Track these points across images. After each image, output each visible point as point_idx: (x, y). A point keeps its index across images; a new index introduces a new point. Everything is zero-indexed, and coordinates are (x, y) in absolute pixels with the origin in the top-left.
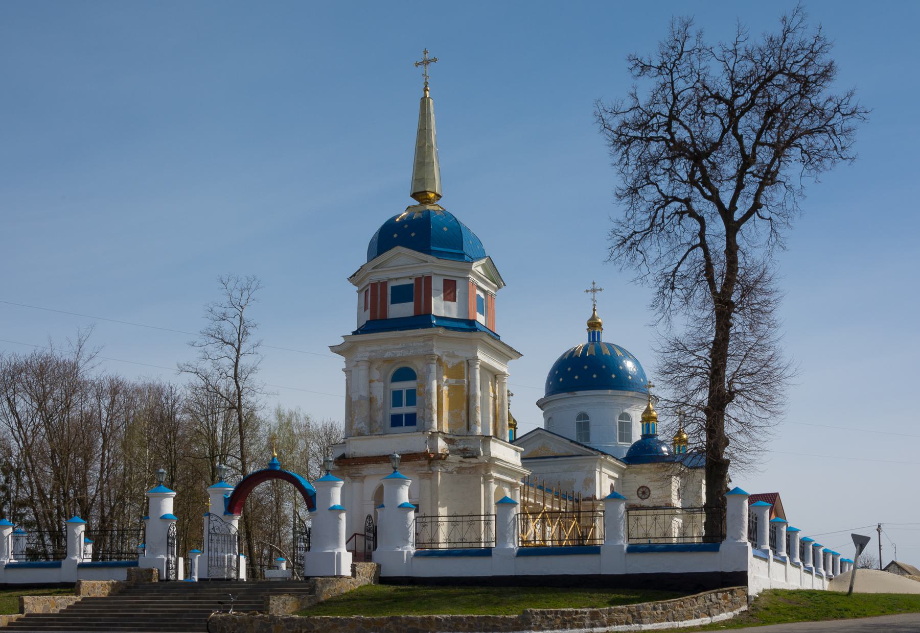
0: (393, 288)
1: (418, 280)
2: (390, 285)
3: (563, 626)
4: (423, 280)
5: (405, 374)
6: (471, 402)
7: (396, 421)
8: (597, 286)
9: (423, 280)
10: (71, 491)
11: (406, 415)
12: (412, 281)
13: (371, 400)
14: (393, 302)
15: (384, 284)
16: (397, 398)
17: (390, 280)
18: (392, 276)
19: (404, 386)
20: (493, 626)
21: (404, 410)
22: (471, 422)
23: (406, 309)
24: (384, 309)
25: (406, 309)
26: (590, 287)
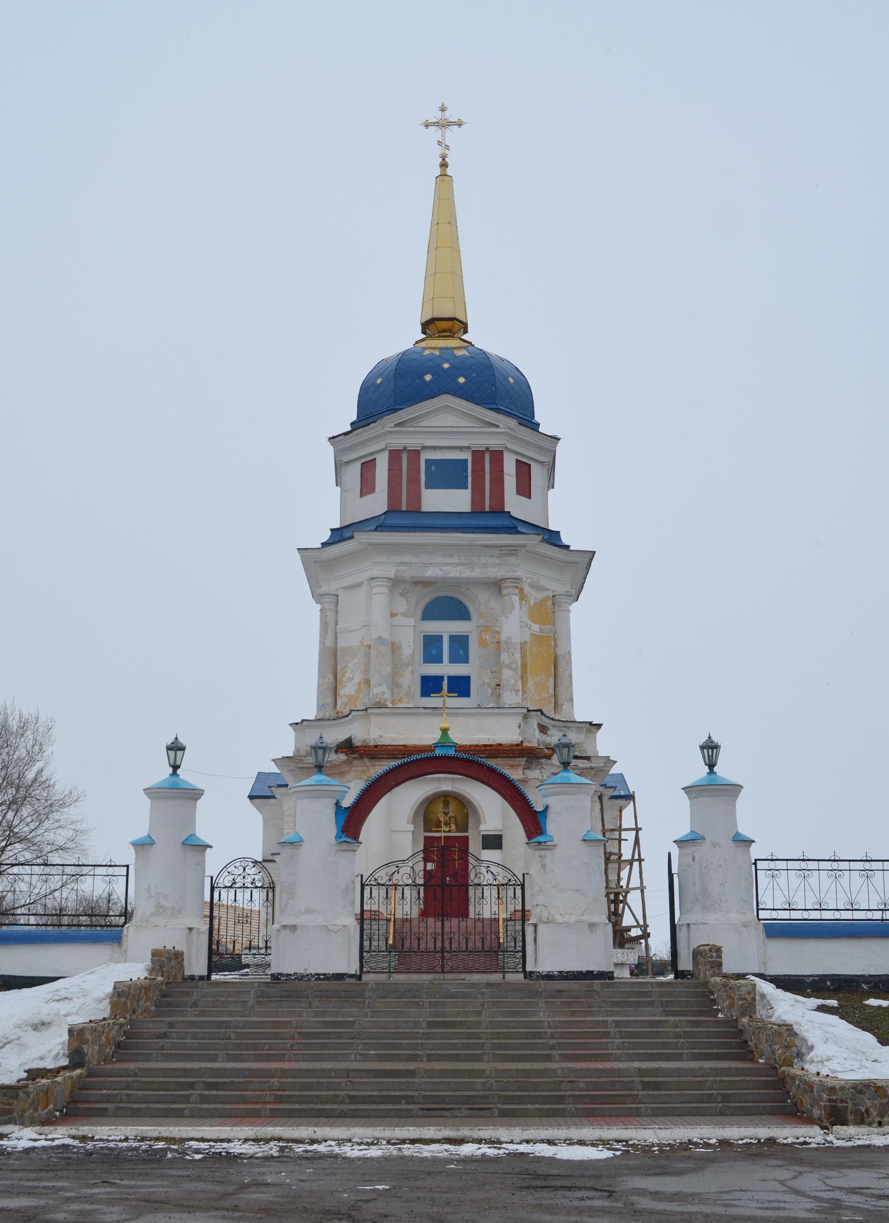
0: (427, 460)
1: (478, 455)
2: (425, 456)
3: (824, 978)
4: (487, 457)
5: (447, 605)
6: (562, 665)
7: (430, 685)
8: (452, 115)
9: (487, 457)
10: (38, 792)
11: (450, 678)
12: (467, 456)
13: (395, 648)
14: (427, 488)
15: (414, 455)
16: (431, 648)
17: (425, 448)
18: (428, 443)
19: (446, 628)
20: (28, 1154)
21: (446, 669)
22: (562, 697)
23: (458, 500)
24: (415, 496)
25: (458, 500)
26: (435, 115)
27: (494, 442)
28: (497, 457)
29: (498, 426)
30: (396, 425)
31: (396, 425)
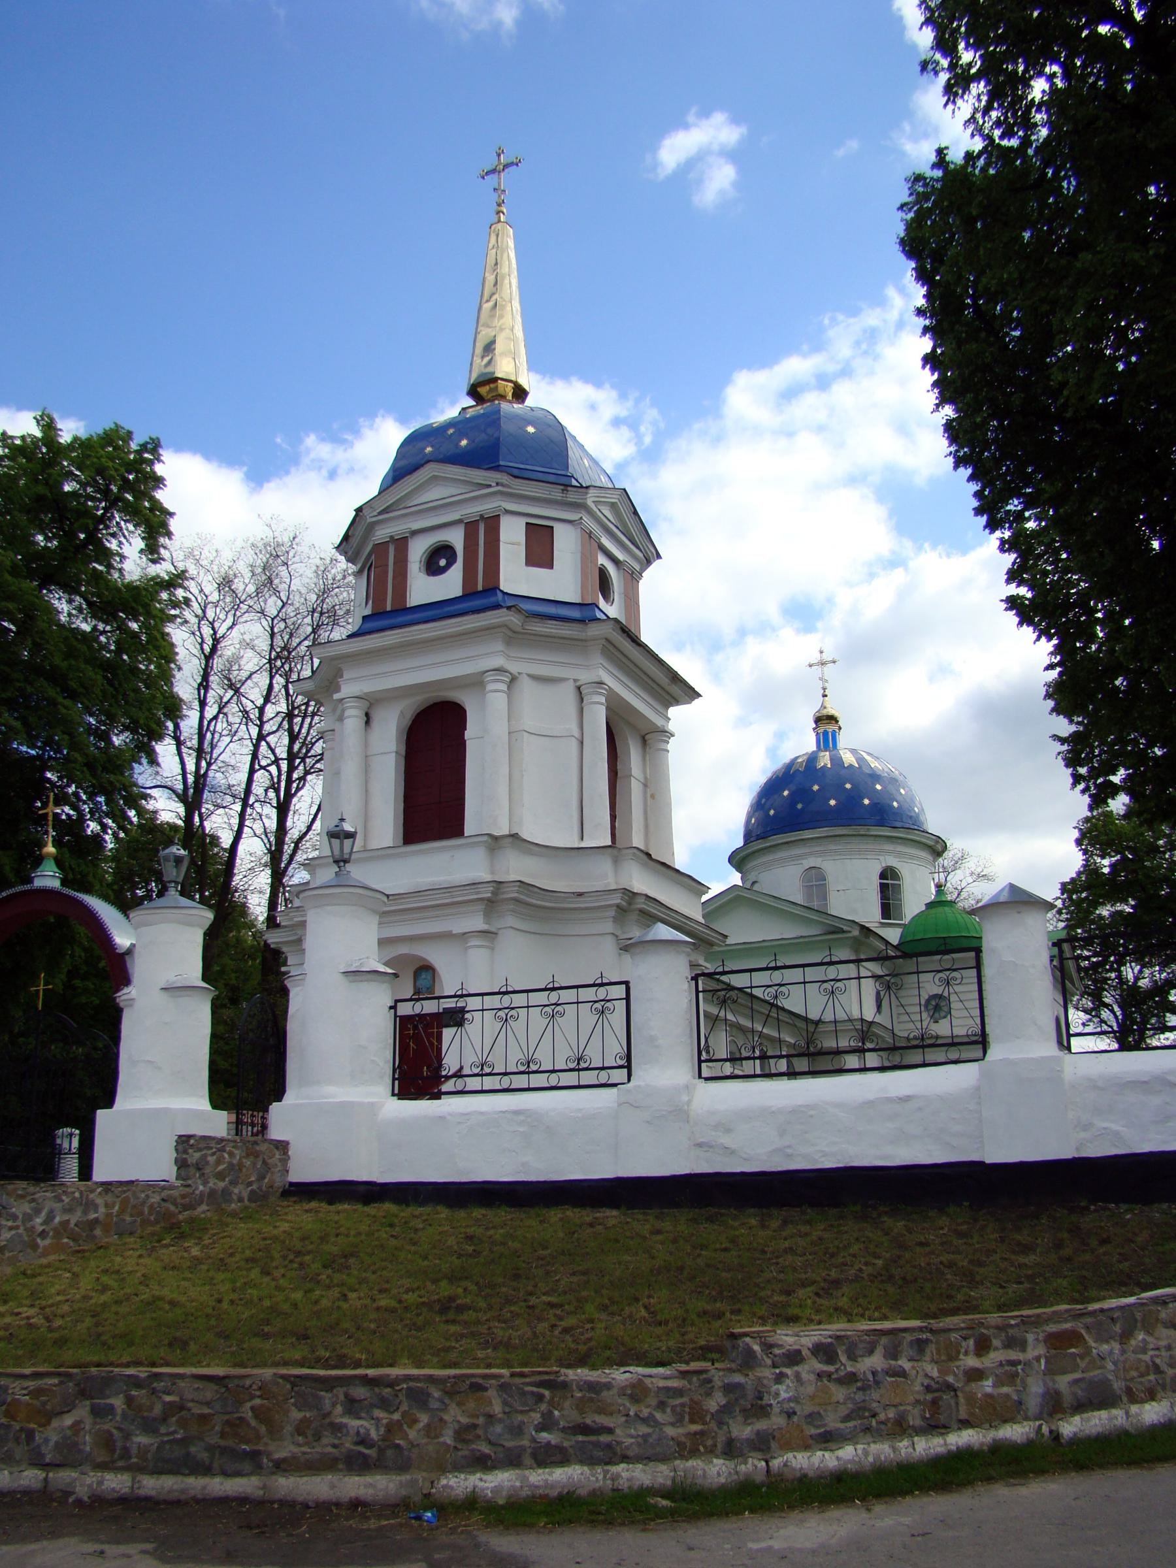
27: (486, 507)
28: (492, 523)
29: (490, 486)
30: (380, 513)
31: (380, 513)
